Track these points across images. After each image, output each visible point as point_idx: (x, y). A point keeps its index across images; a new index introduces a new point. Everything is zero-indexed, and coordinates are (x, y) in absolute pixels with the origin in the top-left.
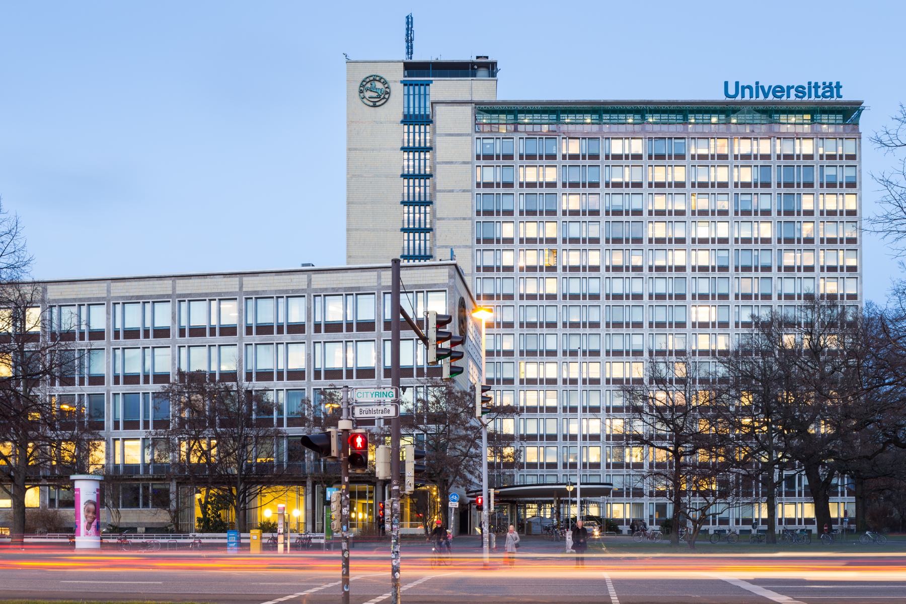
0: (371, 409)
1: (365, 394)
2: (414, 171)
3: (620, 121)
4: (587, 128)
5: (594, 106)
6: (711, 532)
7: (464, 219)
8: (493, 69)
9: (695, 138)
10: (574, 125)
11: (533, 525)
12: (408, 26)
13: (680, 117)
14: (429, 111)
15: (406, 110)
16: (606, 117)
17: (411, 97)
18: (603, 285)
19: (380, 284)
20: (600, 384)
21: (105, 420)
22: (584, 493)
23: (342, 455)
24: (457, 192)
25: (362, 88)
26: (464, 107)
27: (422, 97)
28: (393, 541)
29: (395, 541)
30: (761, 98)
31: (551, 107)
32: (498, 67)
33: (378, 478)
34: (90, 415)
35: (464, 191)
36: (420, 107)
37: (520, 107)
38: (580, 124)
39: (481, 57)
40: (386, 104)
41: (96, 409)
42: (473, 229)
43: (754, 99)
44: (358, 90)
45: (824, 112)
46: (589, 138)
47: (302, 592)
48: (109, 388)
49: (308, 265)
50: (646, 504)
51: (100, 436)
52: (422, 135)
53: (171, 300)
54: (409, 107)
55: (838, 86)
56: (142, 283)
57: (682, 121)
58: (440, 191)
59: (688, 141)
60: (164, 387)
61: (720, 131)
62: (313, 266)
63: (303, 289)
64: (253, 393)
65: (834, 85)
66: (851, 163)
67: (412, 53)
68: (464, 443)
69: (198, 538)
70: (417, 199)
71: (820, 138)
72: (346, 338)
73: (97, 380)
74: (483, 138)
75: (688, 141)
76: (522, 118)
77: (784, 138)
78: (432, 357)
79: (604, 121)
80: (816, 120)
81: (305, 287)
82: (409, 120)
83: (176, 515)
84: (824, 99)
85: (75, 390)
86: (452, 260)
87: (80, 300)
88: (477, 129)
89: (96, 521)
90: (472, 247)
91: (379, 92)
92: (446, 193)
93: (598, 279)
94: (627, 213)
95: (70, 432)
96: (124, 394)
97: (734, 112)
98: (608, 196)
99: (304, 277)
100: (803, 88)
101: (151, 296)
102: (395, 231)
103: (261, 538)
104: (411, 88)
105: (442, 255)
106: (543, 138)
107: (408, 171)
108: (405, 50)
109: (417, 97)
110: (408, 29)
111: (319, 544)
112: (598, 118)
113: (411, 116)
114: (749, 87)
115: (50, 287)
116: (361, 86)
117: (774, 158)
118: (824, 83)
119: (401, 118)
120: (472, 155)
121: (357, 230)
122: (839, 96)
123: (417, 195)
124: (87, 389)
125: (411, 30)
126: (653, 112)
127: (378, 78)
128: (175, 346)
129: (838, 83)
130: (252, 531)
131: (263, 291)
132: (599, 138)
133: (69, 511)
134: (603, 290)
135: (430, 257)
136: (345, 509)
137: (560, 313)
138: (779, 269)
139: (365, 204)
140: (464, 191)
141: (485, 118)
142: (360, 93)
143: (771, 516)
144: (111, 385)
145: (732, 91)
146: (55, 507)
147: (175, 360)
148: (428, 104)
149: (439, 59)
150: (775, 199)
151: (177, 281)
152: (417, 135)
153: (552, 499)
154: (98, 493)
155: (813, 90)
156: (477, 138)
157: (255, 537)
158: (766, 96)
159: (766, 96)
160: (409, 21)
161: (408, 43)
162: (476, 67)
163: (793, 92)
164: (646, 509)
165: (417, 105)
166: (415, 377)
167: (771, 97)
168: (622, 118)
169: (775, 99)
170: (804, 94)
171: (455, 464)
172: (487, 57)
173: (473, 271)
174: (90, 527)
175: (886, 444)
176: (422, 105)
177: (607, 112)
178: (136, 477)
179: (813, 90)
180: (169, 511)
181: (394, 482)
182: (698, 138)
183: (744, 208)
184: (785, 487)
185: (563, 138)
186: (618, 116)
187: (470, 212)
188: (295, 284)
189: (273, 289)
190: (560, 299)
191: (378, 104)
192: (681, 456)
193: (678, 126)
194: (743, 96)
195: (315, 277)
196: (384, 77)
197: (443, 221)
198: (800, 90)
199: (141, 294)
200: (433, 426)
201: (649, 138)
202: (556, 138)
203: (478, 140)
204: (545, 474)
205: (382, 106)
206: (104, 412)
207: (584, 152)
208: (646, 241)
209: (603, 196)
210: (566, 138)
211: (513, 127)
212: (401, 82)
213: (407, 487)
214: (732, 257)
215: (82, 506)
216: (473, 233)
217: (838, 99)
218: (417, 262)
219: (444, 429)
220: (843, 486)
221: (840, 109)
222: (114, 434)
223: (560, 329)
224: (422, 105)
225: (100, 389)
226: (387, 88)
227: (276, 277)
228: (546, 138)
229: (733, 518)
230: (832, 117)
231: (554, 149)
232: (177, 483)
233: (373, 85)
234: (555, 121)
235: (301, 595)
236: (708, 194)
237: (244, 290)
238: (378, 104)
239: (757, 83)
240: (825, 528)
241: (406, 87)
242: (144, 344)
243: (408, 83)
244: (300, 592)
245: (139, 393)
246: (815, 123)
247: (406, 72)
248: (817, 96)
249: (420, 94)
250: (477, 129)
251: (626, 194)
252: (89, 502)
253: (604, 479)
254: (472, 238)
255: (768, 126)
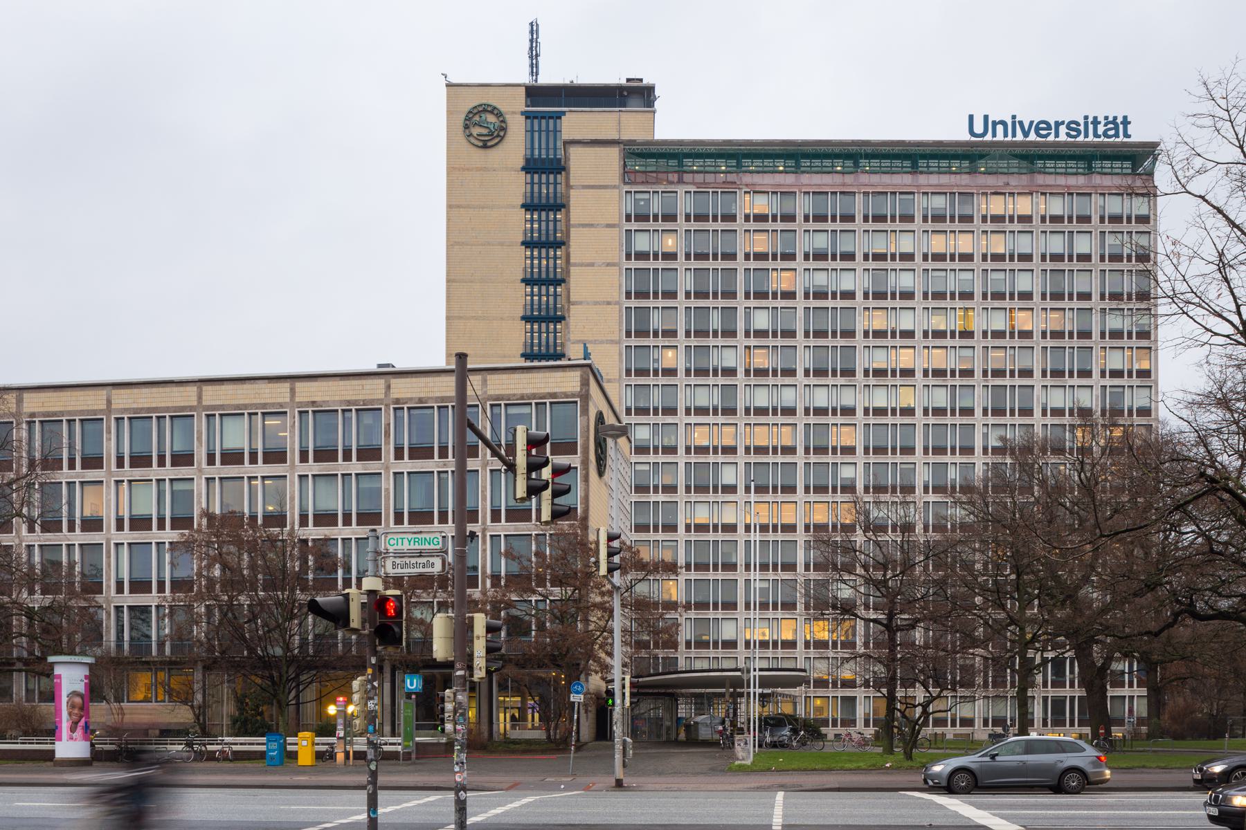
0: (408, 562)
1: (400, 541)
2: (540, 237)
3: (825, 169)
4: (779, 179)
5: (766, 148)
6: (949, 736)
7: (609, 303)
8: (649, 95)
9: (927, 193)
10: (761, 175)
11: (700, 726)
12: (532, 36)
13: (907, 163)
14: (562, 152)
15: (529, 152)
16: (805, 163)
17: (536, 135)
18: (800, 394)
19: (486, 392)
20: (796, 532)
21: (104, 580)
22: (764, 682)
23: (367, 625)
24: (599, 266)
25: (468, 122)
26: (608, 149)
27: (551, 134)
28: (456, 748)
29: (459, 747)
30: (1020, 137)
31: (729, 150)
32: (657, 93)
33: (435, 659)
34: (82, 574)
35: (608, 265)
36: (548, 149)
37: (686, 149)
38: (769, 172)
39: (633, 79)
40: (501, 144)
41: (91, 565)
42: (621, 316)
43: (1009, 138)
44: (462, 124)
45: (1105, 157)
46: (781, 192)
47: (345, 818)
48: (109, 535)
49: (388, 365)
50: (860, 698)
51: (97, 602)
52: (551, 187)
53: (195, 413)
54: (532, 149)
55: (1126, 122)
56: (155, 390)
57: (910, 169)
58: (575, 265)
59: (978, 199)
60: (183, 535)
61: (963, 183)
62: (393, 367)
63: (378, 400)
64: (310, 544)
65: (1119, 120)
66: (1142, 228)
67: (537, 74)
68: (599, 614)
69: (226, 744)
70: (544, 276)
71: (1100, 194)
72: (439, 467)
73: (92, 524)
74: (635, 192)
75: (919, 198)
76: (690, 164)
77: (1050, 193)
78: (521, 491)
79: (920, 169)
80: (1095, 168)
81: (382, 396)
82: (532, 167)
83: (201, 713)
84: (1106, 140)
85: (63, 537)
86: (585, 359)
87: (69, 413)
88: (627, 180)
89: (83, 719)
90: (619, 342)
91: (492, 127)
92: (583, 268)
93: (794, 388)
94: (834, 296)
95: (51, 596)
96: (130, 544)
97: (982, 157)
98: (807, 272)
99: (380, 382)
100: (1078, 124)
101: (168, 407)
102: (514, 320)
103: (313, 744)
104: (536, 122)
105: (574, 353)
106: (717, 192)
107: (532, 236)
108: (528, 69)
109: (543, 134)
110: (531, 41)
111: (397, 753)
112: (852, 165)
113: (535, 160)
114: (1003, 123)
115: (27, 396)
116: (466, 120)
117: (1037, 221)
118: (1106, 118)
119: (521, 163)
120: (620, 214)
121: (460, 318)
122: (1127, 135)
123: (544, 269)
124: (79, 537)
125: (537, 42)
126: (869, 156)
127: (489, 109)
128: (201, 478)
129: (1125, 118)
130: (300, 734)
131: (324, 401)
132: (795, 193)
133: (45, 707)
134: (801, 401)
135: (561, 356)
136: (372, 702)
137: (740, 434)
138: (747, 372)
139: (472, 282)
140: (608, 265)
141: (638, 163)
142: (465, 128)
143: (1024, 714)
144: (112, 532)
145: (979, 128)
146: (35, 702)
147: (201, 497)
148: (560, 144)
149: (575, 82)
150: (1037, 277)
151: (205, 388)
152: (544, 187)
153: (724, 690)
154: (87, 681)
155: (1091, 127)
156: (626, 192)
157: (305, 743)
158: (1026, 134)
159: (1026, 134)
160: (534, 29)
161: (532, 60)
162: (625, 93)
163: (1063, 129)
164: (860, 704)
165: (543, 146)
166: (533, 522)
167: (1033, 137)
168: (827, 164)
169: (1039, 139)
170: (1079, 132)
171: (587, 642)
172: (641, 80)
173: (620, 376)
174: (76, 728)
175: (1176, 615)
176: (551, 146)
177: (807, 156)
178: (147, 660)
179: (1091, 127)
180: (192, 707)
181: (458, 665)
182: (932, 193)
183: (996, 290)
184: (1052, 675)
185: (745, 192)
186: (881, 163)
187: (616, 294)
188: (368, 392)
189: (337, 398)
190: (741, 415)
191: (489, 144)
192: (897, 630)
193: (905, 176)
194: (994, 135)
195: (396, 383)
196: (498, 107)
197: (579, 306)
198: (1072, 126)
199: (154, 405)
200: (557, 590)
201: (864, 193)
202: (736, 192)
203: (629, 195)
204: (720, 656)
205: (497, 147)
206: (102, 569)
207: (775, 212)
208: (859, 335)
209: (800, 272)
210: (749, 192)
211: (676, 175)
212: (523, 113)
213: (475, 672)
214: (978, 357)
215: (64, 699)
216: (620, 323)
217: (1126, 140)
218: (536, 363)
219: (573, 592)
220: (1131, 672)
221: (1129, 154)
222: (115, 600)
223: (741, 456)
224: (551, 146)
225: (97, 537)
226: (502, 121)
227: (342, 383)
228: (722, 192)
229: (979, 718)
230: (1117, 164)
231: (734, 208)
232: (204, 667)
233: (484, 118)
234: (735, 169)
235: (342, 824)
236: (946, 270)
237: (297, 400)
238: (489, 144)
239: (1014, 117)
240: (1101, 731)
241: (529, 121)
242: (158, 475)
243: (532, 115)
244: (341, 819)
245: (151, 543)
246: (1094, 172)
247: (529, 99)
248: (1096, 135)
249: (548, 131)
250: (627, 180)
251: (832, 269)
252: (75, 693)
253: (801, 664)
254: (620, 330)
255: (1029, 176)
